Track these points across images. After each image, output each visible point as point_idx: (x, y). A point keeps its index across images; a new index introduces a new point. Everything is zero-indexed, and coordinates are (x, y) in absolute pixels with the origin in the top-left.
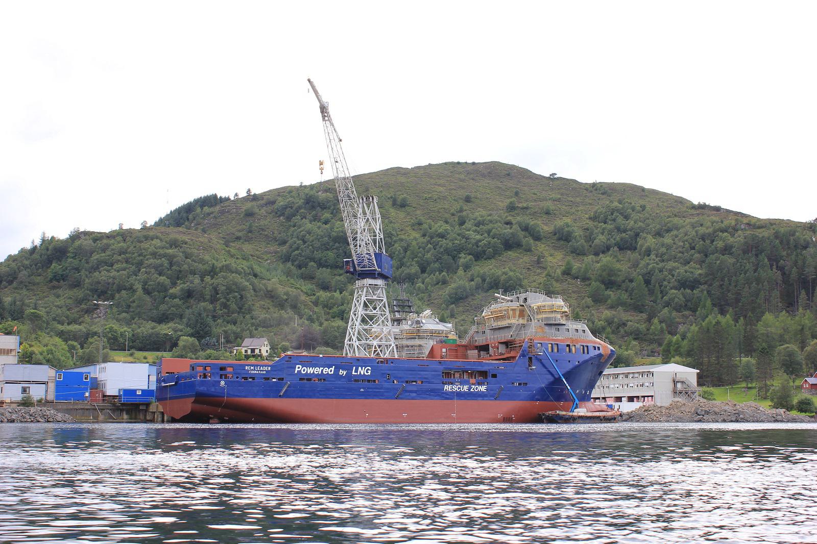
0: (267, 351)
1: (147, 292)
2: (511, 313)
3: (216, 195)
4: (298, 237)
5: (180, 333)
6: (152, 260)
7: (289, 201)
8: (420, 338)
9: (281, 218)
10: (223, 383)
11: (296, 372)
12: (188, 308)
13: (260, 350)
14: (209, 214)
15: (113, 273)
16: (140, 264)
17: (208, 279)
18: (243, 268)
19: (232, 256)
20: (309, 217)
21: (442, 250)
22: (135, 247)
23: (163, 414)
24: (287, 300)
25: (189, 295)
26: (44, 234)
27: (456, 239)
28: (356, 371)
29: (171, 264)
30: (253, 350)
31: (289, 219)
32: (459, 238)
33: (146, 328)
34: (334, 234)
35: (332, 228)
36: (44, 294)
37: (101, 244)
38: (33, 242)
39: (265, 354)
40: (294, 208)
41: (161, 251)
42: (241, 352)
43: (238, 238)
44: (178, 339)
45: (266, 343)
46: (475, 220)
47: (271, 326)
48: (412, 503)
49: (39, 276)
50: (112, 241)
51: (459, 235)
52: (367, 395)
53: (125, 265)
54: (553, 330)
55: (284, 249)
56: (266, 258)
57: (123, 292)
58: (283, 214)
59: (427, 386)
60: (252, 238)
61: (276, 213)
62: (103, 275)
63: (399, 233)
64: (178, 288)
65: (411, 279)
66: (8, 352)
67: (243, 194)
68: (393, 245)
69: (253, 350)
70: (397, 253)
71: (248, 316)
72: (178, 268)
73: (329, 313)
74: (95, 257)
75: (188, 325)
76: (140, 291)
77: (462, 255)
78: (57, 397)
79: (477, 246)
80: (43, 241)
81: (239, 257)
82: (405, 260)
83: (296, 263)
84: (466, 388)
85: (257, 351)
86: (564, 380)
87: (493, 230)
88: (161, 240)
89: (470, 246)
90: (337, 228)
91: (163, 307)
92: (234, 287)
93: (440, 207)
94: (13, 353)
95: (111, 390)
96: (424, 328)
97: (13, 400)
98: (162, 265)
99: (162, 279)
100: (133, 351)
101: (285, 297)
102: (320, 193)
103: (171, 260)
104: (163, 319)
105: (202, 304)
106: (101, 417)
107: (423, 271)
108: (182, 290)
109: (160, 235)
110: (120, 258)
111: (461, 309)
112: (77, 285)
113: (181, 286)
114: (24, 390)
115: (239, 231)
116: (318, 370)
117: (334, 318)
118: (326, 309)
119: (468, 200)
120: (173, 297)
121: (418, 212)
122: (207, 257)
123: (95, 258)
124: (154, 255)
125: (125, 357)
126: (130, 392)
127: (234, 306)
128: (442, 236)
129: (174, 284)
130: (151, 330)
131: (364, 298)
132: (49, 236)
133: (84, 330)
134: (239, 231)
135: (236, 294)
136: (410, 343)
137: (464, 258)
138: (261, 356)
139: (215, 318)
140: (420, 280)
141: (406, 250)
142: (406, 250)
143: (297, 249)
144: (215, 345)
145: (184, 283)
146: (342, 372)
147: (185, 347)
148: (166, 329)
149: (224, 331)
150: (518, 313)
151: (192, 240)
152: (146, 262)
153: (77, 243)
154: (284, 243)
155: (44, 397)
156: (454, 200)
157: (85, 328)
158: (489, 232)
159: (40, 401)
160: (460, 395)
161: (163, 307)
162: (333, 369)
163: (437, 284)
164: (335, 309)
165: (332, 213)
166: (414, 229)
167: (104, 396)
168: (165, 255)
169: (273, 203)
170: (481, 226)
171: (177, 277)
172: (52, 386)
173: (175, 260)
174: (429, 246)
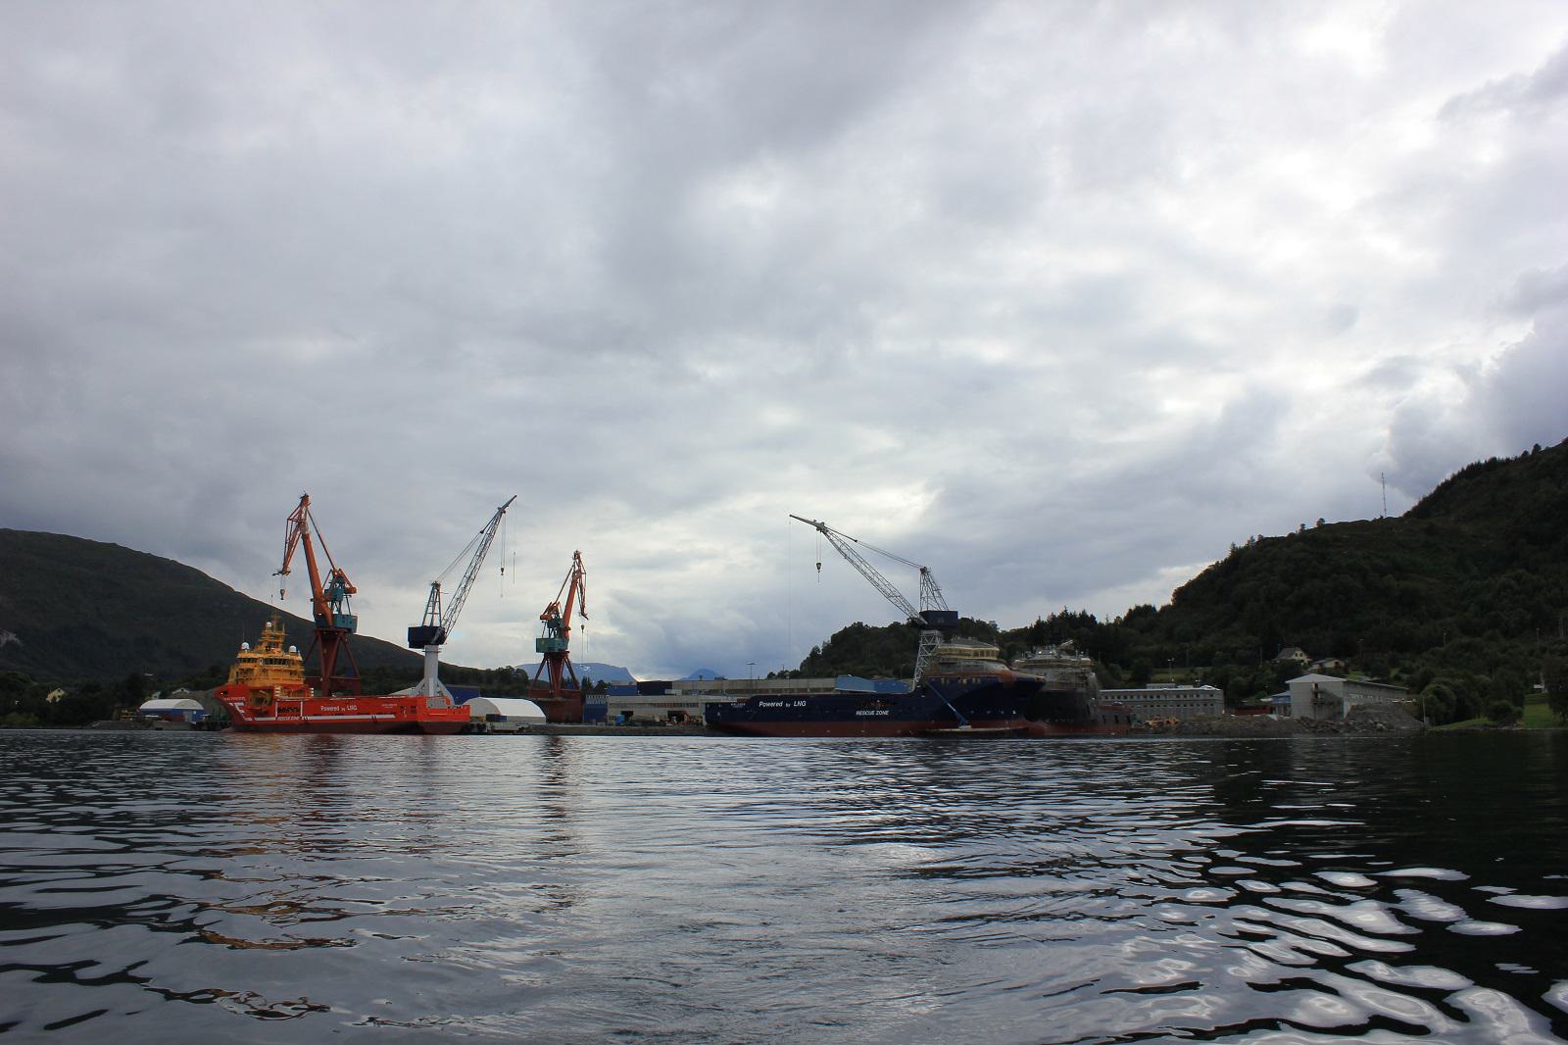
84: (872, 713)
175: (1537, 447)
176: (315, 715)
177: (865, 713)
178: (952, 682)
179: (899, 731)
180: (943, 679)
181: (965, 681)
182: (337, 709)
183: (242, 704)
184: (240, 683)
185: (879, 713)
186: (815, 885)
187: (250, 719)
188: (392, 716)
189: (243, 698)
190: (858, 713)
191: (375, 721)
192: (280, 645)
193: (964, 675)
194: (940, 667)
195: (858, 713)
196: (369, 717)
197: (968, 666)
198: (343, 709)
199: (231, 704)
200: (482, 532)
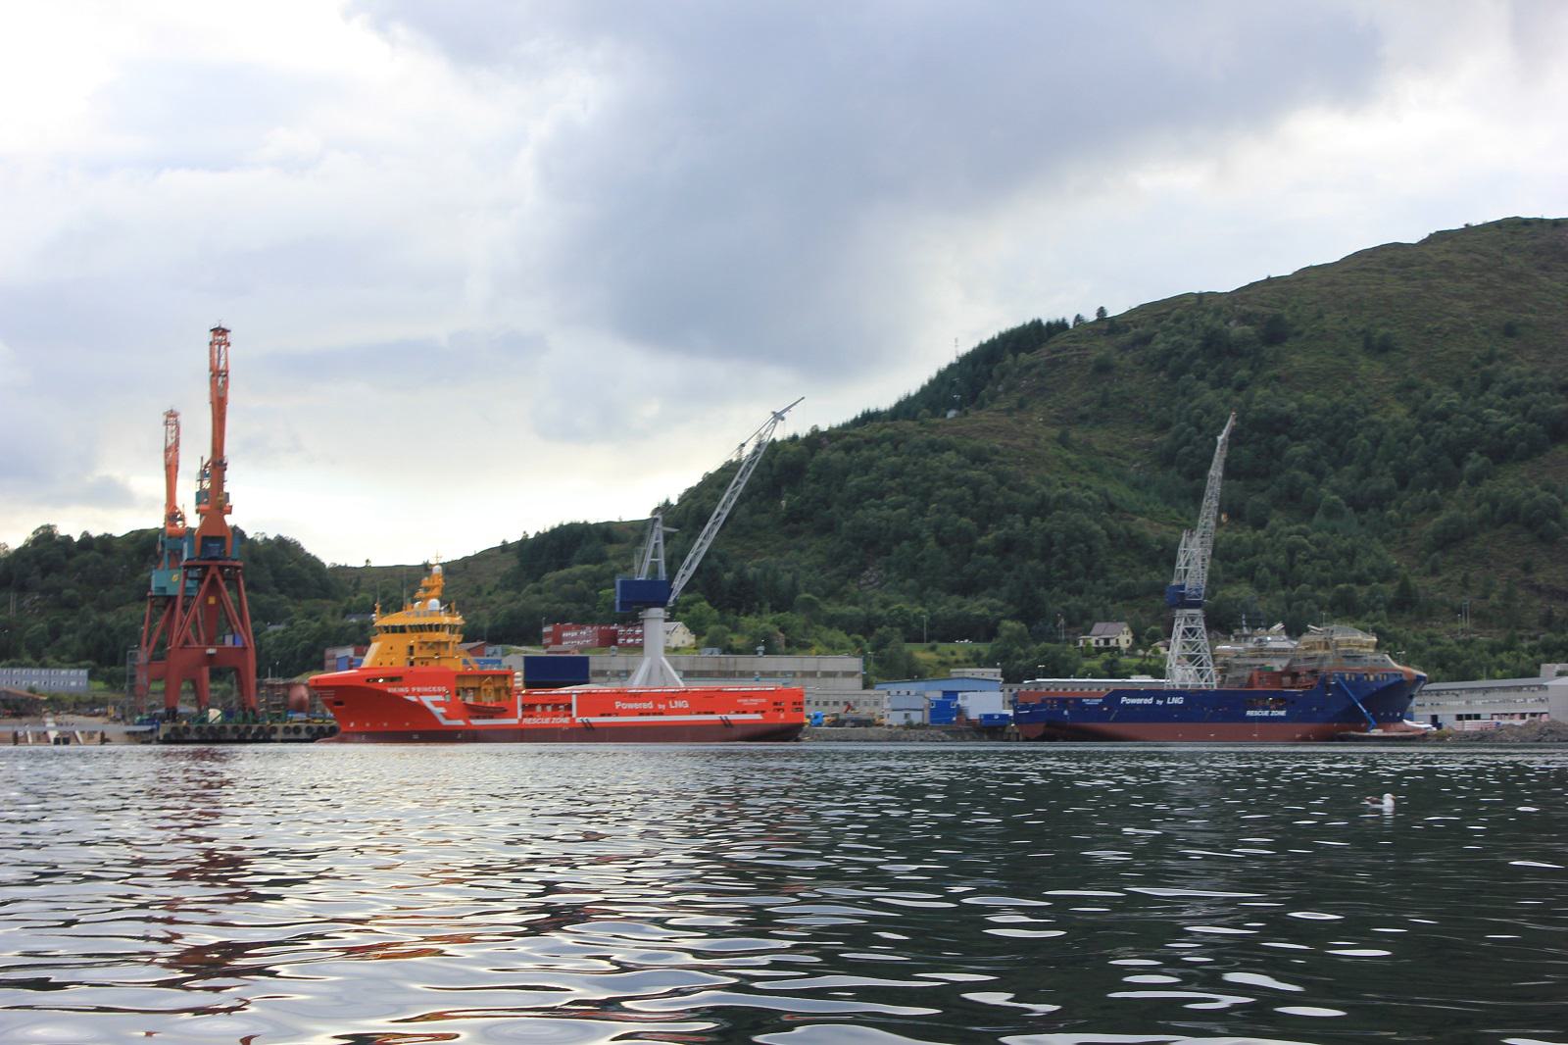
0: (1128, 641)
1: (942, 543)
2: (1317, 644)
3: (1039, 321)
4: (1188, 419)
5: (999, 614)
6: (945, 490)
7: (1175, 341)
8: (1263, 656)
9: (1162, 374)
10: (1066, 712)
12: (1009, 568)
13: (1117, 640)
14: (1029, 368)
15: (886, 512)
16: (926, 496)
17: (1036, 521)
18: (1090, 498)
19: (1074, 468)
20: (1211, 374)
21: (1438, 445)
22: (915, 464)
23: (1018, 734)
24: (1162, 551)
25: (1006, 546)
27: (1465, 424)
29: (977, 496)
30: (1107, 641)
31: (1175, 376)
32: (1471, 420)
33: (950, 606)
34: (1251, 415)
35: (1248, 402)
36: (778, 545)
37: (858, 457)
39: (1124, 645)
40: (1184, 357)
41: (960, 474)
42: (1089, 644)
43: (1084, 418)
44: (997, 622)
46: (1505, 382)
47: (1137, 597)
49: (764, 512)
50: (876, 452)
51: (1471, 415)
52: (1179, 720)
53: (901, 498)
54: (1351, 662)
55: (1164, 439)
56: (1133, 457)
57: (905, 543)
58: (1163, 367)
60: (1108, 416)
61: (1152, 364)
62: (870, 515)
63: (1370, 407)
64: (990, 537)
65: (1380, 500)
66: (851, 674)
68: (1356, 436)
69: (1107, 641)
70: (1360, 450)
71: (1100, 582)
72: (987, 503)
73: (1231, 569)
74: (853, 481)
75: (1010, 601)
76: (931, 543)
77: (1474, 455)
78: (932, 722)
79: (1502, 438)
81: (1085, 468)
82: (1375, 462)
83: (1185, 469)
84: (1266, 713)
85: (1113, 643)
86: (1360, 706)
87: (1534, 406)
88: (958, 452)
89: (1488, 437)
90: (1257, 404)
91: (968, 568)
92: (1077, 533)
93: (1454, 349)
94: (858, 675)
95: (974, 714)
96: (1268, 646)
97: (900, 723)
98: (962, 498)
99: (965, 521)
100: (934, 643)
101: (1159, 547)
103: (976, 486)
104: (968, 588)
105: (1030, 563)
106: (968, 738)
107: (1403, 483)
108: (996, 538)
109: (952, 437)
110: (892, 484)
111: (1451, 558)
112: (828, 528)
113: (994, 534)
114: (906, 716)
115: (1086, 403)
116: (1139, 701)
117: (1240, 577)
118: (1226, 562)
119: (1510, 331)
120: (984, 551)
121: (1411, 362)
122: (1032, 482)
123: (853, 483)
124: (949, 480)
125: (924, 651)
126: (989, 717)
127: (1078, 566)
128: (1443, 416)
129: (983, 530)
130: (956, 611)
131: (1182, 627)
133: (863, 613)
134: (1086, 403)
135: (1082, 545)
136: (1253, 662)
137: (1475, 461)
138: (1118, 649)
139: (1049, 586)
140: (1393, 503)
141: (1376, 443)
142: (1376, 443)
143: (1187, 442)
144: (1051, 633)
145: (999, 528)
146: (1160, 702)
147: (1009, 639)
148: (977, 607)
149: (1064, 607)
150: (1323, 645)
151: (1006, 445)
152: (938, 493)
153: (821, 455)
154: (1164, 426)
156: (1485, 333)
157: (864, 609)
158: (1525, 409)
159: (918, 725)
160: (1262, 719)
161: (968, 568)
162: (1151, 699)
163: (1423, 509)
164: (1241, 563)
165: (1251, 368)
166: (1398, 399)
167: (967, 720)
168: (966, 481)
169: (1146, 340)
170: (1514, 398)
171: (989, 517)
172: (927, 712)
173: (983, 488)
174: (1418, 437)
175: (1101, 311)
176: (603, 715)
177: (1257, 713)
178: (1356, 679)
179: (1298, 736)
180: (1347, 675)
181: (1372, 678)
182: (649, 705)
183: (440, 698)
184: (417, 663)
185: (1274, 713)
186: (310, 937)
187: (461, 723)
188: (758, 717)
189: (444, 689)
190: (1250, 713)
191: (727, 724)
192: (436, 592)
193: (1373, 671)
194: (1345, 661)
195: (1250, 713)
196: (715, 717)
197: (1375, 660)
198: (662, 707)
199: (413, 699)
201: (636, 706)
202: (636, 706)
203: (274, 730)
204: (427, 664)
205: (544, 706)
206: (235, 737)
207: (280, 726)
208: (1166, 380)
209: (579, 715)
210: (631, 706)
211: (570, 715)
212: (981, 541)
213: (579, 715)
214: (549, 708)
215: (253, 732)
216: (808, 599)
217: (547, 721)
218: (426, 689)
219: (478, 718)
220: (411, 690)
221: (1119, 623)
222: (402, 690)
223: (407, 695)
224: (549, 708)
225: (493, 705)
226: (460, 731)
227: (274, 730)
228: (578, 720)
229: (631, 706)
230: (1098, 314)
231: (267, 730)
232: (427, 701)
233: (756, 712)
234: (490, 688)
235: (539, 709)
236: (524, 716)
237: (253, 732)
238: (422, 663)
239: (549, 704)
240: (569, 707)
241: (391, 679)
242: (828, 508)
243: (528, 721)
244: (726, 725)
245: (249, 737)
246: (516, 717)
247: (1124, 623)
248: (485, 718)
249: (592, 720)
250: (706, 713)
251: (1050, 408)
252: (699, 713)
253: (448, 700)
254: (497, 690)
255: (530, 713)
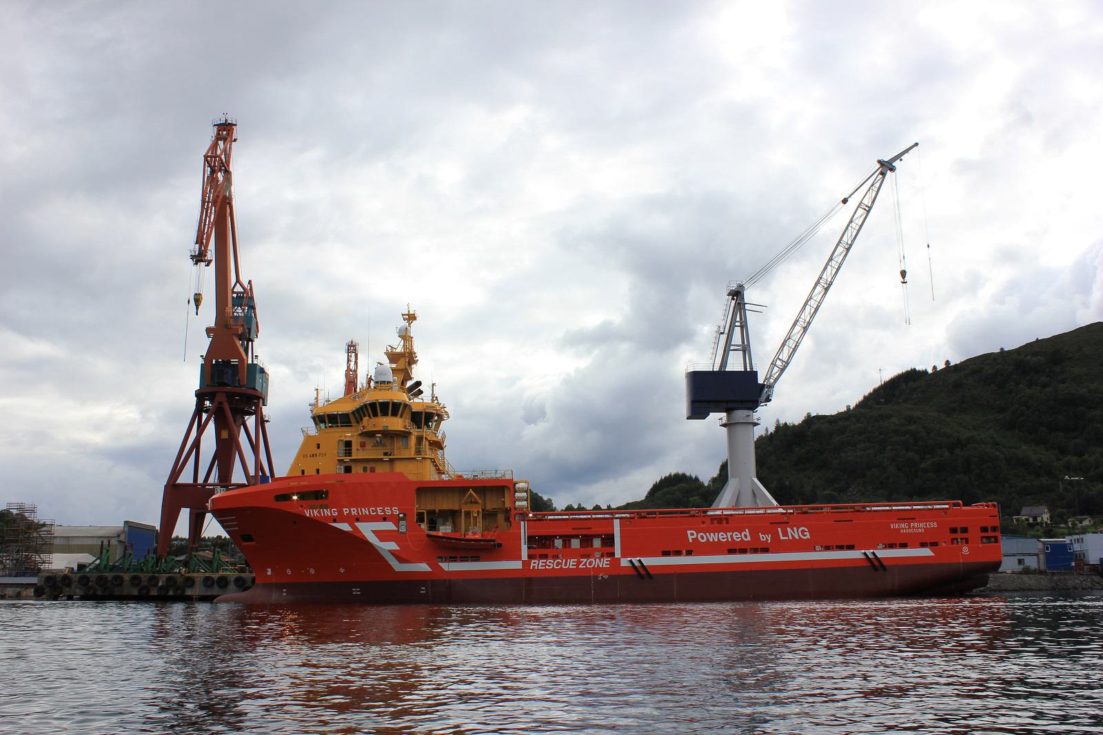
9: (992, 386)
11: (691, 541)
17: (958, 451)
26: (778, 421)
28: (785, 534)
30: (1035, 519)
38: (767, 430)
45: (1046, 511)
48: (280, 692)
50: (848, 423)
59: (104, 551)
64: (929, 463)
67: (941, 366)
69: (1035, 519)
80: (778, 428)
85: (1039, 519)
101: (1039, 464)
102: (1029, 357)
114: (1020, 562)
132: (782, 422)
155: (1037, 567)
172: (1041, 556)
176: (666, 554)
183: (390, 526)
184: (357, 469)
187: (424, 567)
188: (926, 552)
191: (876, 565)
196: (856, 554)
198: (765, 538)
199: (345, 527)
200: (845, 201)
201: (722, 537)
202: (722, 537)
203: (190, 582)
204: (373, 470)
205: (567, 539)
206: (135, 592)
207: (200, 575)
208: (996, 388)
209: (624, 555)
210: (713, 537)
211: (612, 554)
212: (923, 465)
213: (624, 555)
214: (575, 543)
215: (160, 584)
216: (829, 494)
217: (571, 564)
218: (365, 511)
219: (453, 559)
220: (340, 512)
221: (1041, 507)
222: (327, 512)
223: (335, 521)
224: (575, 543)
225: (477, 537)
226: (424, 583)
227: (190, 582)
228: (625, 562)
229: (713, 537)
230: (945, 364)
231: (180, 580)
232: (367, 530)
233: (923, 545)
234: (476, 510)
235: (558, 543)
236: (531, 557)
237: (160, 584)
238: (365, 469)
239: (576, 537)
240: (608, 540)
241: (315, 495)
242: (822, 454)
243: (538, 564)
244: (875, 569)
245: (154, 592)
246: (519, 558)
247: (1044, 507)
248: (464, 559)
249: (648, 561)
250: (841, 548)
251: (932, 406)
252: (827, 548)
253: (403, 529)
254: (489, 515)
255: (544, 551)
